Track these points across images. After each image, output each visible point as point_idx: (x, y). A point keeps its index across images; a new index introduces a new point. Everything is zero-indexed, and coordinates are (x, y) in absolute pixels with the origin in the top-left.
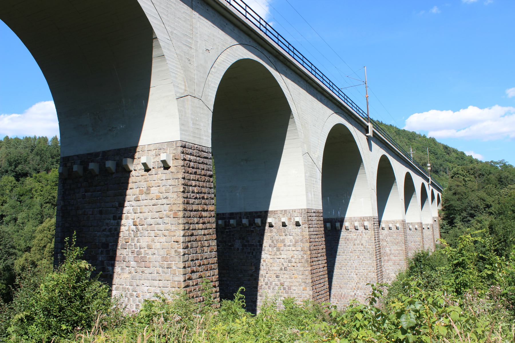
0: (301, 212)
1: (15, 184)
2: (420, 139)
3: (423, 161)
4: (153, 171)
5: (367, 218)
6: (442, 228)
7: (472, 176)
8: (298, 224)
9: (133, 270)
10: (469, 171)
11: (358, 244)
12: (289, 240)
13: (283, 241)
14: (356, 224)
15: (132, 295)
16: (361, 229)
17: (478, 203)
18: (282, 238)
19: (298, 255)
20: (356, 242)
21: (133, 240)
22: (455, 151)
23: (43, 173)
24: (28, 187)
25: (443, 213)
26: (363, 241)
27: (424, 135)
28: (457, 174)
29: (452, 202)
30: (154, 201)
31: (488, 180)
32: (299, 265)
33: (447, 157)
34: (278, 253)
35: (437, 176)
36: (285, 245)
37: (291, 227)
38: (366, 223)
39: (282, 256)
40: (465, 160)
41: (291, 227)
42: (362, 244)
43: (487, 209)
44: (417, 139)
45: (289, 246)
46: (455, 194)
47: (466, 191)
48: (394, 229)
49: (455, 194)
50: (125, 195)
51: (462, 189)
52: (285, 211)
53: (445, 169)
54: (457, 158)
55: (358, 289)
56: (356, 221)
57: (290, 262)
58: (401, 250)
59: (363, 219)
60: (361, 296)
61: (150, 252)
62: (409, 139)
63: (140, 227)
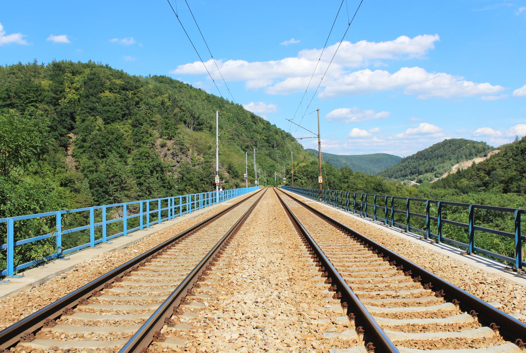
3: (247, 144)
22: (261, 120)
27: (232, 102)
33: (254, 127)
44: (226, 106)
53: (256, 142)
54: (264, 128)
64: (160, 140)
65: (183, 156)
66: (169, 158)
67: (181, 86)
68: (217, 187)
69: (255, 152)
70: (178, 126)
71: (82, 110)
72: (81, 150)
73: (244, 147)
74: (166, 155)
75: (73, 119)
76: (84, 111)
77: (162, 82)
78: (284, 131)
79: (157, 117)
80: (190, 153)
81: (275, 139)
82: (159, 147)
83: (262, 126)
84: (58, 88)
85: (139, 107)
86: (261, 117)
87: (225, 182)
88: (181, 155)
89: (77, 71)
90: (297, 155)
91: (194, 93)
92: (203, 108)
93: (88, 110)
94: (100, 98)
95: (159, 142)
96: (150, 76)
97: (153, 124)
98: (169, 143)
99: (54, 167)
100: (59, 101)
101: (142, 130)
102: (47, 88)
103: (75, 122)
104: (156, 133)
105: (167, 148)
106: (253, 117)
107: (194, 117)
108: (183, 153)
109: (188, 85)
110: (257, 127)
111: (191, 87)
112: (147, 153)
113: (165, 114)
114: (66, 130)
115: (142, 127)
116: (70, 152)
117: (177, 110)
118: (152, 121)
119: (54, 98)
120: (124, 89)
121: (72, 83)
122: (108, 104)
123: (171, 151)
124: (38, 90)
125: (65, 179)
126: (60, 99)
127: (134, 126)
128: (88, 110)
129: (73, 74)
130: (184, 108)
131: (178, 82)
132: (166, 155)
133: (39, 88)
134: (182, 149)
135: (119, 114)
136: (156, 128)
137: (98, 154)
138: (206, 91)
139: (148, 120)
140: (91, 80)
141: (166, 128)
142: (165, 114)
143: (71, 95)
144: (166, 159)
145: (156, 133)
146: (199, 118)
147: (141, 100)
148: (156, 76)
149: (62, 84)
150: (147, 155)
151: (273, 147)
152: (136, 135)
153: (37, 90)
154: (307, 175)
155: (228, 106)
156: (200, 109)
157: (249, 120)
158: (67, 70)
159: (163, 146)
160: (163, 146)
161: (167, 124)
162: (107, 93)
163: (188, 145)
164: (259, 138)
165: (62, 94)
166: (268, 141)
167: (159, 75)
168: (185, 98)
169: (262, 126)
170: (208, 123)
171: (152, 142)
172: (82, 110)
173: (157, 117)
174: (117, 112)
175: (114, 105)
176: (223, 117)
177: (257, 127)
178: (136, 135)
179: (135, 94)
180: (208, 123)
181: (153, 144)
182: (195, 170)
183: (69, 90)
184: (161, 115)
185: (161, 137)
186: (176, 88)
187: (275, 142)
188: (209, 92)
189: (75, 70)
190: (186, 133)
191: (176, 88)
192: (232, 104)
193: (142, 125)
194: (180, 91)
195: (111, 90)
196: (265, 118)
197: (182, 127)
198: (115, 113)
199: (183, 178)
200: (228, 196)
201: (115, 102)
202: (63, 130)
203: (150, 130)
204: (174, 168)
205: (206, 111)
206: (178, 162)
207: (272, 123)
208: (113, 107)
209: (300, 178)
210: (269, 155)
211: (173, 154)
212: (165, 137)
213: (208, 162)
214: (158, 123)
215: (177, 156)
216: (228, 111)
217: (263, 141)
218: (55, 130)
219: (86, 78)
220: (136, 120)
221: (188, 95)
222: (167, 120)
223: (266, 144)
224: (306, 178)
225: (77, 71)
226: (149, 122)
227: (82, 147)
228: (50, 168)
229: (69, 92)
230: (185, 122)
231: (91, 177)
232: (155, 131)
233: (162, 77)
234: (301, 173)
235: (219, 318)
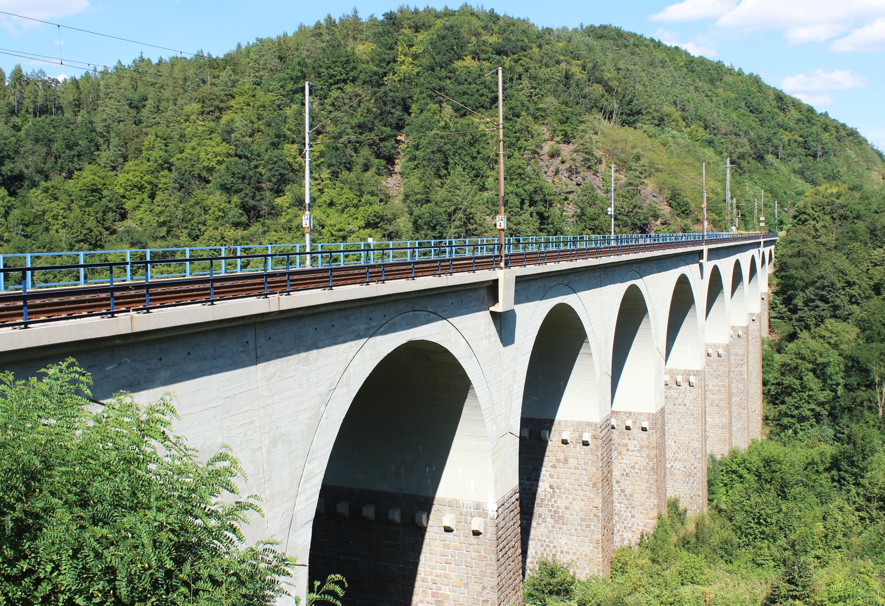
0: (649, 416)
1: (9, 201)
2: (731, 78)
3: (741, 150)
4: (571, 445)
5: (693, 371)
6: (773, 308)
7: (828, 218)
8: (644, 429)
9: (550, 525)
10: (823, 209)
11: (679, 405)
12: (632, 445)
13: (626, 445)
14: (679, 379)
15: (548, 546)
16: (685, 385)
17: (834, 278)
18: (624, 442)
19: (642, 461)
20: (677, 402)
21: (549, 500)
22: (796, 104)
23: (57, 179)
24: (37, 209)
25: (776, 281)
26: (687, 402)
27: (740, 69)
28: (804, 213)
29: (792, 272)
30: (573, 471)
31: (854, 233)
32: (643, 472)
33: (780, 118)
34: (619, 457)
35: (762, 167)
36: (627, 450)
37: (636, 431)
38: (692, 379)
39: (625, 461)
40: (814, 124)
41: (636, 431)
42: (685, 405)
43: (847, 289)
44: (726, 78)
45: (633, 451)
46: (798, 254)
47: (817, 253)
48: (714, 355)
49: (798, 254)
50: (542, 461)
51: (812, 248)
52: (630, 413)
53: (776, 147)
54: (799, 120)
55: (676, 460)
56: (678, 374)
57: (633, 467)
58: (723, 386)
59: (688, 373)
60: (679, 470)
61: (567, 512)
62: (712, 81)
63: (557, 491)
65: (589, 175)
66: (564, 177)
67: (637, 42)
71: (422, 93)
72: (412, 164)
73: (735, 157)
74: (557, 173)
75: (407, 109)
76: (424, 95)
79: (550, 102)
81: (820, 141)
82: (546, 157)
84: (384, 56)
86: (794, 96)
87: (662, 224)
89: (424, 25)
93: (430, 92)
94: (453, 71)
95: (547, 148)
96: (582, 26)
98: (566, 150)
99: (358, 193)
100: (385, 79)
102: (365, 57)
103: (410, 114)
109: (652, 40)
110: (786, 119)
113: (564, 96)
114: (389, 129)
115: (519, 120)
116: (398, 169)
119: (375, 74)
120: (499, 53)
121: (411, 46)
122: (466, 80)
123: (567, 165)
124: (349, 62)
125: (375, 215)
126: (385, 74)
128: (430, 92)
129: (417, 29)
132: (557, 173)
133: (351, 58)
134: (589, 160)
135: (484, 98)
136: (546, 122)
137: (438, 170)
140: (443, 38)
141: (562, 123)
142: (564, 96)
143: (405, 68)
144: (556, 180)
145: (544, 131)
146: (631, 101)
149: (391, 48)
150: (519, 171)
151: (815, 156)
153: (348, 62)
154: (832, 212)
157: (769, 105)
158: (405, 23)
159: (553, 155)
160: (553, 155)
162: (468, 61)
164: (786, 139)
165: (389, 67)
166: (805, 145)
167: (597, 25)
172: (422, 93)
173: (550, 102)
174: (482, 95)
175: (478, 82)
176: (714, 99)
179: (516, 61)
183: (403, 58)
184: (557, 97)
187: (820, 146)
189: (419, 22)
190: (603, 133)
192: (740, 73)
195: (476, 56)
196: (805, 100)
197: (596, 120)
198: (476, 96)
201: (479, 76)
202: (384, 129)
206: (578, 185)
207: (819, 110)
208: (474, 85)
209: (814, 219)
211: (570, 170)
215: (577, 173)
216: (731, 87)
217: (795, 145)
218: (371, 130)
219: (435, 36)
224: (828, 218)
225: (424, 25)
227: (414, 158)
228: (351, 195)
229: (403, 62)
231: (417, 211)
233: (603, 27)
234: (818, 209)
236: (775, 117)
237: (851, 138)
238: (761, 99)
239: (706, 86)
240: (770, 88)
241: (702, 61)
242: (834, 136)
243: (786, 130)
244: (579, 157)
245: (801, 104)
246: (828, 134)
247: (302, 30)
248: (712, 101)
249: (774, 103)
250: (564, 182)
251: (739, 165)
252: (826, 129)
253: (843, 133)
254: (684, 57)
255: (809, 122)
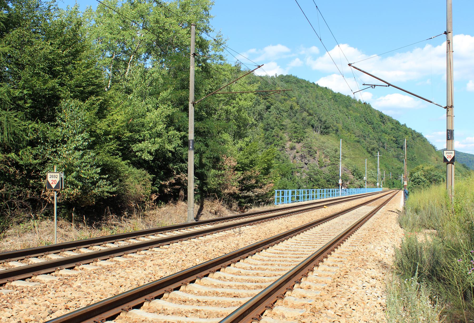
2: (355, 105)
3: (373, 146)
27: (360, 100)
33: (383, 127)
44: (352, 104)
53: (383, 143)
54: (392, 128)
62: (347, 107)
64: (290, 143)
65: (311, 159)
66: (298, 160)
67: (307, 85)
68: (340, 187)
69: (379, 155)
70: (306, 130)
73: (369, 149)
74: (295, 157)
77: (288, 82)
78: (414, 131)
79: (286, 122)
80: (317, 155)
82: (288, 149)
83: (391, 126)
85: (270, 112)
87: (350, 184)
88: (308, 157)
90: (429, 157)
91: (320, 93)
92: (330, 108)
95: (288, 144)
97: (283, 127)
98: (298, 146)
101: (274, 134)
104: (286, 137)
105: (296, 150)
106: (382, 116)
107: (321, 121)
108: (311, 155)
109: (314, 83)
110: (386, 127)
111: (317, 86)
112: (278, 155)
113: (294, 119)
117: (305, 114)
118: (282, 125)
123: (300, 154)
127: (266, 130)
130: (311, 111)
131: (304, 81)
132: (295, 157)
134: (310, 151)
136: (285, 131)
138: (333, 90)
139: (278, 124)
141: (295, 132)
145: (286, 137)
146: (325, 121)
147: (272, 105)
148: (282, 75)
150: (278, 157)
152: (267, 138)
155: (355, 106)
156: (329, 113)
157: (376, 120)
159: (292, 148)
160: (292, 148)
161: (296, 128)
163: (315, 148)
166: (396, 142)
168: (312, 97)
169: (391, 126)
170: (335, 126)
171: (283, 145)
176: (350, 117)
177: (386, 127)
178: (267, 138)
180: (335, 126)
181: (283, 147)
182: (322, 171)
185: (290, 140)
186: (302, 87)
188: (336, 90)
190: (314, 138)
191: (302, 87)
193: (273, 129)
194: (306, 91)
199: (310, 178)
200: (336, 194)
203: (281, 134)
204: (302, 169)
205: (333, 112)
206: (306, 164)
207: (402, 123)
210: (398, 157)
212: (294, 141)
213: (334, 164)
214: (288, 126)
215: (305, 158)
216: (356, 110)
217: (392, 142)
220: (268, 124)
221: (314, 95)
222: (296, 125)
223: (394, 145)
226: (279, 126)
230: (313, 126)
232: (285, 135)
233: (288, 76)
235: (340, 316)
236: (380, 126)
237: (419, 138)
238: (372, 117)
239: (345, 110)
240: (376, 111)
241: (340, 95)
242: (411, 137)
243: (386, 133)
244: (306, 150)
245: (393, 120)
246: (407, 136)
247: (405, 125)
248: (348, 118)
249: (379, 119)
250: (298, 162)
251: (372, 153)
252: (406, 133)
253: (415, 136)
254: (330, 93)
255: (398, 129)
